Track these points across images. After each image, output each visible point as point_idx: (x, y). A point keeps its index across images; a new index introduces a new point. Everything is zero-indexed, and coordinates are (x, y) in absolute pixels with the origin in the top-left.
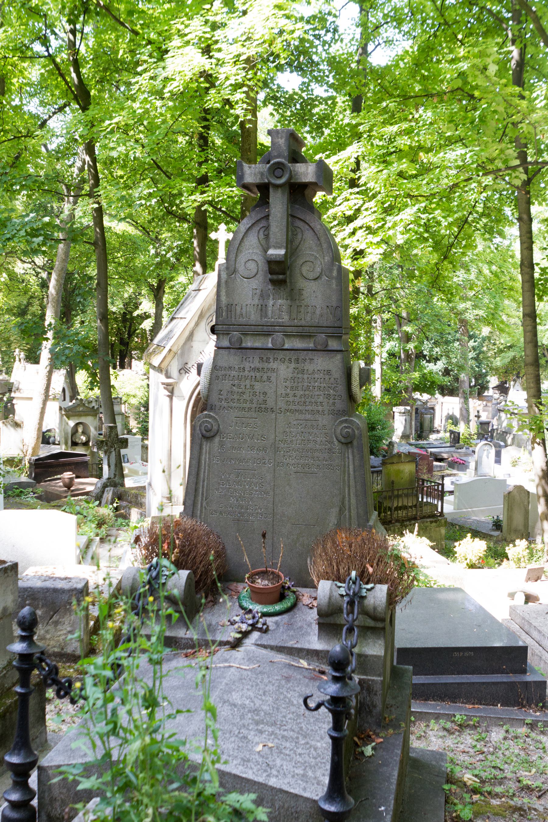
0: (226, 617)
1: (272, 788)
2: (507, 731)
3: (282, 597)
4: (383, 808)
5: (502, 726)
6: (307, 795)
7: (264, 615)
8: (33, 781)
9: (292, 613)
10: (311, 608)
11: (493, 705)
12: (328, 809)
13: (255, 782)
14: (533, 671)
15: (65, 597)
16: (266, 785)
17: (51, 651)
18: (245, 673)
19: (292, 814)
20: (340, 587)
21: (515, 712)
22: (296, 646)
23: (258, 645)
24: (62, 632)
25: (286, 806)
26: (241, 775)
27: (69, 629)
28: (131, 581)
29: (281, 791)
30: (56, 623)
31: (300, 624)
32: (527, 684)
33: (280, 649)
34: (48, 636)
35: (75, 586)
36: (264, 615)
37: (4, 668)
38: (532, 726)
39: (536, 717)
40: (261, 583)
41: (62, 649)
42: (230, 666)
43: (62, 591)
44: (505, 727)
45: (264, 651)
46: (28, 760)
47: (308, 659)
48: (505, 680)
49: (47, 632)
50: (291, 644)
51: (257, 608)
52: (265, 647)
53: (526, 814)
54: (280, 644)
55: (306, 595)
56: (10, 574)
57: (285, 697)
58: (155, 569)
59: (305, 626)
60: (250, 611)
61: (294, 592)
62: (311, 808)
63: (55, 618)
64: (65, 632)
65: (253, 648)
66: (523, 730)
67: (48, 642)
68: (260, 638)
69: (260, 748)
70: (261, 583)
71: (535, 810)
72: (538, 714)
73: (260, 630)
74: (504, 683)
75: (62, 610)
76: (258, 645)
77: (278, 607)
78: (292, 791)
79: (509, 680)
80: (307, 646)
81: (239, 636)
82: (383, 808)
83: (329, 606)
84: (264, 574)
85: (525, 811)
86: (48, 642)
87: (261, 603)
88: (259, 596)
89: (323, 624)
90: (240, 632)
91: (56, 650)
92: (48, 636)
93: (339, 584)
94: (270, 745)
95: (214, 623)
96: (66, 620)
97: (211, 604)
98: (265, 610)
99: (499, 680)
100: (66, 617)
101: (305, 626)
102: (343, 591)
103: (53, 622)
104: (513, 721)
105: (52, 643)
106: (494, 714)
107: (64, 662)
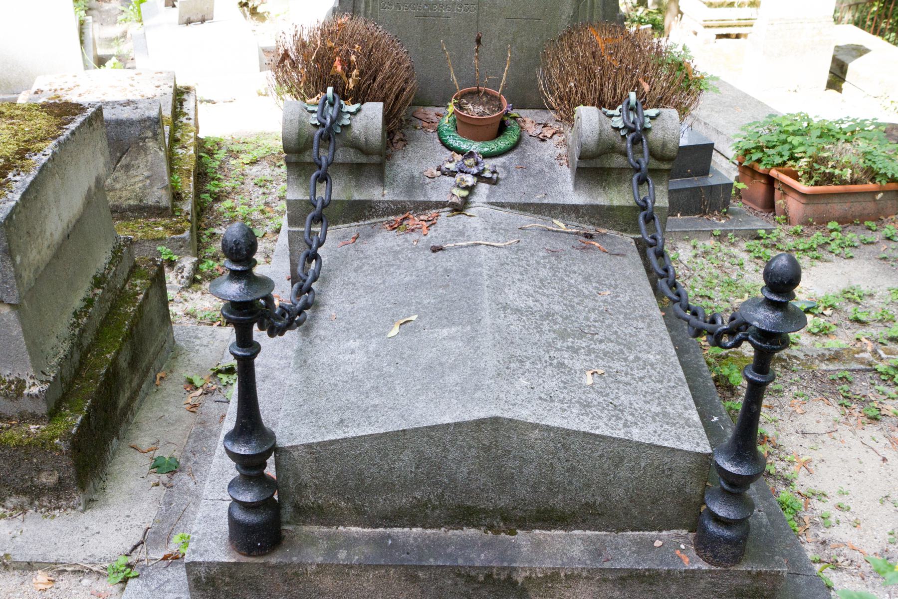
0: (426, 163)
1: (638, 444)
2: (694, 247)
3: (502, 128)
4: (716, 419)
5: (688, 240)
6: (686, 447)
7: (487, 156)
8: (270, 470)
9: (518, 150)
10: (543, 140)
11: (672, 215)
12: (728, 469)
13: (614, 439)
14: (717, 173)
15: (135, 131)
16: (630, 441)
17: (125, 204)
18: (501, 252)
19: (664, 471)
20: (612, 116)
21: (697, 222)
22: (546, 201)
23: (492, 204)
24: (137, 179)
25: (656, 463)
26: (593, 432)
27: (146, 174)
28: (297, 125)
29: (652, 446)
30: (127, 167)
31: (537, 167)
32: (712, 188)
33: (524, 208)
34: (118, 186)
35: (147, 114)
36: (487, 156)
37: (110, 263)
38: (721, 238)
39: (723, 225)
40: (474, 110)
41: (141, 201)
42: (476, 245)
43: (130, 123)
44: (692, 242)
45: (504, 213)
46: (264, 450)
47: (563, 218)
48: (688, 186)
49: (116, 180)
50: (536, 199)
51: (475, 147)
52: (502, 205)
53: (788, 364)
54: (523, 201)
55: (528, 120)
56: (95, 125)
57: (570, 286)
58: (332, 105)
59: (546, 170)
60: (471, 154)
61: (515, 118)
62: (692, 463)
63: (124, 161)
64: (141, 178)
65: (487, 209)
66: (710, 243)
67: (118, 194)
68: (492, 193)
69: (589, 380)
70: (474, 110)
71: (795, 357)
72: (723, 221)
73: (489, 181)
74: (687, 189)
75: (133, 149)
76: (492, 204)
77: (502, 143)
78: (666, 444)
79: (692, 186)
80: (561, 201)
81: (465, 193)
82: (716, 419)
83: (598, 145)
84: (472, 95)
85: (785, 360)
86: (118, 194)
87: (476, 139)
88: (465, 126)
89: (583, 168)
90: (466, 188)
91: (132, 202)
92: (118, 186)
93: (610, 112)
94: (600, 371)
95: (416, 174)
96: (141, 161)
97: (401, 144)
98: (486, 150)
99: (681, 186)
100: (140, 158)
101: (546, 170)
102: (618, 123)
103: (122, 167)
104: (699, 233)
105: (124, 194)
106: (678, 226)
107: (145, 218)
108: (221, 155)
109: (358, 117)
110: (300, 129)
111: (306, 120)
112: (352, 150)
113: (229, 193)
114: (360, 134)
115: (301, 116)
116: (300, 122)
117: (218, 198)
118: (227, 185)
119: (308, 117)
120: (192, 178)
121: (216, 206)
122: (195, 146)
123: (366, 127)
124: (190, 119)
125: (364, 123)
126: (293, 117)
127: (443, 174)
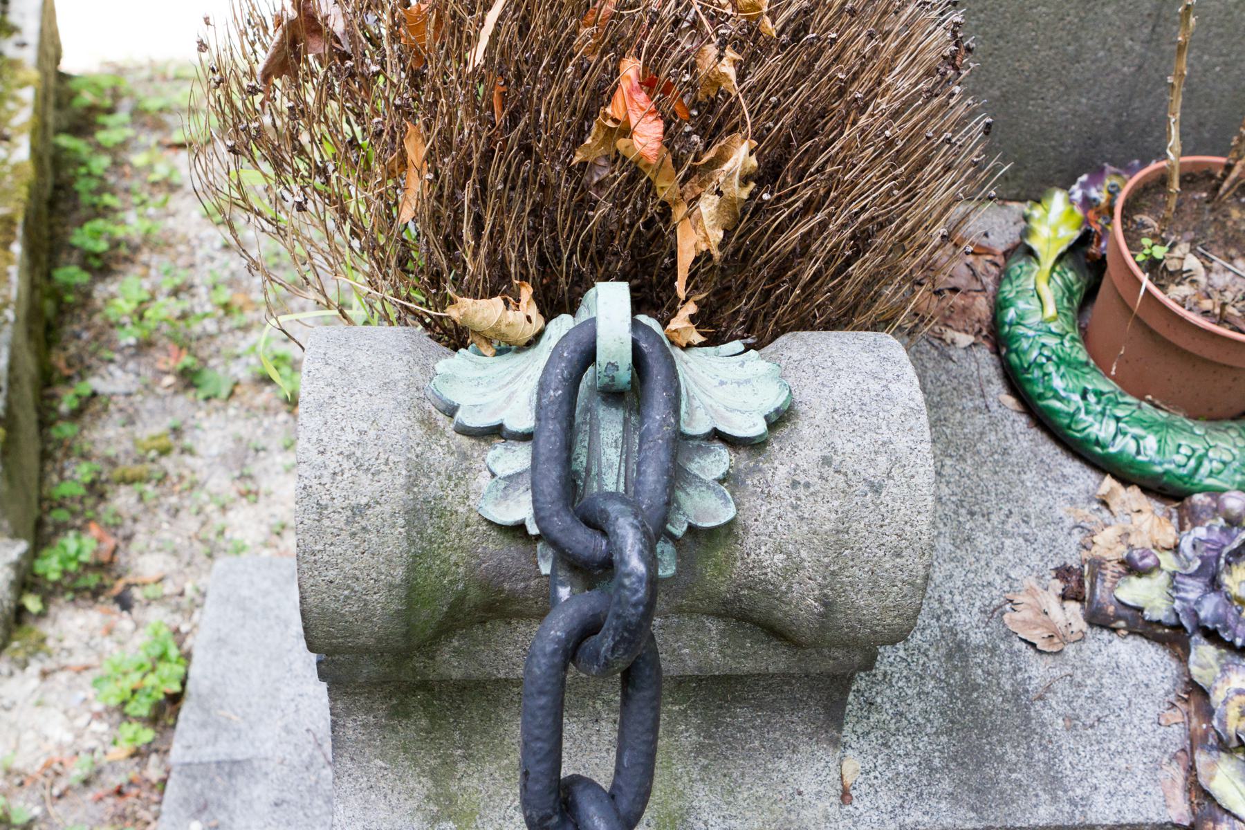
28: (395, 540)
108: (114, 131)
109: (778, 468)
110: (415, 563)
111: (452, 499)
112: (714, 626)
113: (136, 249)
114: (786, 573)
115: (418, 471)
116: (422, 514)
117: (103, 266)
118: (132, 225)
119: (460, 475)
120: (17, 248)
121: (101, 291)
122: (34, 133)
123: (838, 541)
124: (23, 45)
125: (825, 513)
126: (367, 487)
127: (1098, 620)
